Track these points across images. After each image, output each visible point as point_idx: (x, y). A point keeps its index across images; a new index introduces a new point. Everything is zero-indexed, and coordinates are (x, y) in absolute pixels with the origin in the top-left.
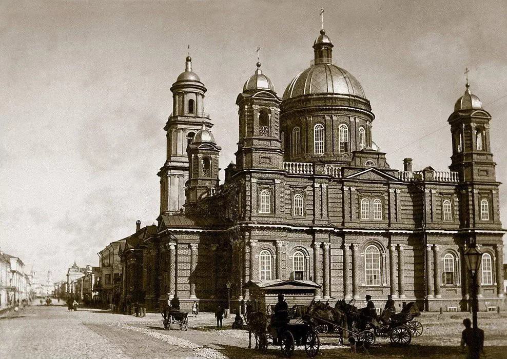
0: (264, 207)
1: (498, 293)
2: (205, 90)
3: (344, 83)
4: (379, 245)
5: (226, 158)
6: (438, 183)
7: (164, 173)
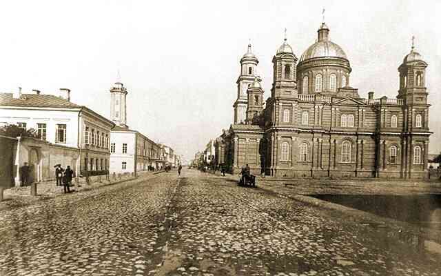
0: (286, 120)
1: (424, 169)
2: (258, 62)
3: (334, 51)
4: (351, 141)
5: (267, 95)
6: (389, 105)
7: (235, 105)
